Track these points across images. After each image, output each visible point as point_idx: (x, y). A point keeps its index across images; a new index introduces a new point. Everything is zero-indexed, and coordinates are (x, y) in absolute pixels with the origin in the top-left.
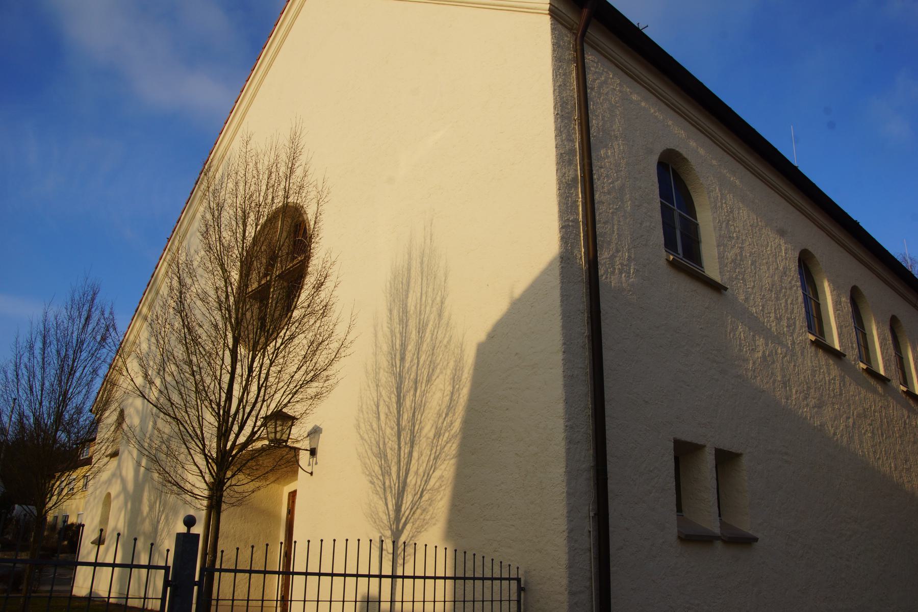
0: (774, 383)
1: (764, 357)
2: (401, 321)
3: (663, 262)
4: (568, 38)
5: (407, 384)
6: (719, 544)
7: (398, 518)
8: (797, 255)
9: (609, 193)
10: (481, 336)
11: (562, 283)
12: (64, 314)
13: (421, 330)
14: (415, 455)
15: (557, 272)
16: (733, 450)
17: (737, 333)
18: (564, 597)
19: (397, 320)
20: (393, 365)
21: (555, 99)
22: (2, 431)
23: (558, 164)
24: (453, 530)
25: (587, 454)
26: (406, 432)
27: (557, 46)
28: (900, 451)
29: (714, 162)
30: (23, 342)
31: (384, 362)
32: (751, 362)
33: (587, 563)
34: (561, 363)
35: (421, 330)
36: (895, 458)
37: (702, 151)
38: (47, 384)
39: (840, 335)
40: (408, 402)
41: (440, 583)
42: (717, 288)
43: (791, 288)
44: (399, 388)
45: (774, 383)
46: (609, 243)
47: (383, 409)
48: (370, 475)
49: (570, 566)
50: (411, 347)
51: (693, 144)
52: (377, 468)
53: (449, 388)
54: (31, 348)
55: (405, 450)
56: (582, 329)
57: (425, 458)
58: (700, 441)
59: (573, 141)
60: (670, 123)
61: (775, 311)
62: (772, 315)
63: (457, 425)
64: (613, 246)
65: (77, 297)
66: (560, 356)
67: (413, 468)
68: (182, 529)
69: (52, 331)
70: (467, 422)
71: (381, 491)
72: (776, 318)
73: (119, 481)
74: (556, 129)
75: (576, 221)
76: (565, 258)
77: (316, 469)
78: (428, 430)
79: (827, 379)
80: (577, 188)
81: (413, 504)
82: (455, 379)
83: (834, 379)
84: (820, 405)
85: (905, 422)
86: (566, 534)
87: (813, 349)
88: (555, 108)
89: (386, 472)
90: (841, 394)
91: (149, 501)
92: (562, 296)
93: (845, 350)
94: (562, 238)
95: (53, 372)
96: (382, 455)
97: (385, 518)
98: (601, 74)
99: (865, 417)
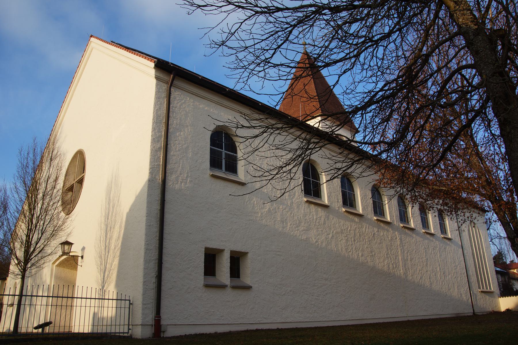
0: (275, 222)
4: (165, 87)
5: (109, 229)
9: (179, 151)
11: (148, 190)
13: (113, 207)
16: (243, 251)
17: (252, 202)
18: (141, 306)
20: (105, 221)
21: (154, 116)
23: (152, 143)
24: (117, 285)
25: (155, 255)
26: (107, 248)
27: (157, 92)
28: (367, 248)
31: (103, 221)
33: (152, 294)
35: (113, 207)
36: (363, 250)
39: (328, 197)
40: (108, 236)
41: (80, 296)
42: (243, 184)
44: (106, 230)
47: (102, 239)
50: (110, 214)
55: (107, 255)
56: (157, 207)
57: (111, 257)
60: (222, 114)
63: (120, 244)
66: (145, 218)
70: (122, 243)
75: (160, 165)
76: (151, 181)
77: (83, 264)
78: (113, 247)
79: (315, 218)
81: (108, 275)
82: (120, 227)
84: (308, 230)
85: (374, 234)
87: (307, 204)
89: (101, 264)
90: (324, 224)
92: (148, 195)
93: (331, 203)
94: (150, 173)
96: (101, 257)
97: (100, 281)
98: (182, 100)
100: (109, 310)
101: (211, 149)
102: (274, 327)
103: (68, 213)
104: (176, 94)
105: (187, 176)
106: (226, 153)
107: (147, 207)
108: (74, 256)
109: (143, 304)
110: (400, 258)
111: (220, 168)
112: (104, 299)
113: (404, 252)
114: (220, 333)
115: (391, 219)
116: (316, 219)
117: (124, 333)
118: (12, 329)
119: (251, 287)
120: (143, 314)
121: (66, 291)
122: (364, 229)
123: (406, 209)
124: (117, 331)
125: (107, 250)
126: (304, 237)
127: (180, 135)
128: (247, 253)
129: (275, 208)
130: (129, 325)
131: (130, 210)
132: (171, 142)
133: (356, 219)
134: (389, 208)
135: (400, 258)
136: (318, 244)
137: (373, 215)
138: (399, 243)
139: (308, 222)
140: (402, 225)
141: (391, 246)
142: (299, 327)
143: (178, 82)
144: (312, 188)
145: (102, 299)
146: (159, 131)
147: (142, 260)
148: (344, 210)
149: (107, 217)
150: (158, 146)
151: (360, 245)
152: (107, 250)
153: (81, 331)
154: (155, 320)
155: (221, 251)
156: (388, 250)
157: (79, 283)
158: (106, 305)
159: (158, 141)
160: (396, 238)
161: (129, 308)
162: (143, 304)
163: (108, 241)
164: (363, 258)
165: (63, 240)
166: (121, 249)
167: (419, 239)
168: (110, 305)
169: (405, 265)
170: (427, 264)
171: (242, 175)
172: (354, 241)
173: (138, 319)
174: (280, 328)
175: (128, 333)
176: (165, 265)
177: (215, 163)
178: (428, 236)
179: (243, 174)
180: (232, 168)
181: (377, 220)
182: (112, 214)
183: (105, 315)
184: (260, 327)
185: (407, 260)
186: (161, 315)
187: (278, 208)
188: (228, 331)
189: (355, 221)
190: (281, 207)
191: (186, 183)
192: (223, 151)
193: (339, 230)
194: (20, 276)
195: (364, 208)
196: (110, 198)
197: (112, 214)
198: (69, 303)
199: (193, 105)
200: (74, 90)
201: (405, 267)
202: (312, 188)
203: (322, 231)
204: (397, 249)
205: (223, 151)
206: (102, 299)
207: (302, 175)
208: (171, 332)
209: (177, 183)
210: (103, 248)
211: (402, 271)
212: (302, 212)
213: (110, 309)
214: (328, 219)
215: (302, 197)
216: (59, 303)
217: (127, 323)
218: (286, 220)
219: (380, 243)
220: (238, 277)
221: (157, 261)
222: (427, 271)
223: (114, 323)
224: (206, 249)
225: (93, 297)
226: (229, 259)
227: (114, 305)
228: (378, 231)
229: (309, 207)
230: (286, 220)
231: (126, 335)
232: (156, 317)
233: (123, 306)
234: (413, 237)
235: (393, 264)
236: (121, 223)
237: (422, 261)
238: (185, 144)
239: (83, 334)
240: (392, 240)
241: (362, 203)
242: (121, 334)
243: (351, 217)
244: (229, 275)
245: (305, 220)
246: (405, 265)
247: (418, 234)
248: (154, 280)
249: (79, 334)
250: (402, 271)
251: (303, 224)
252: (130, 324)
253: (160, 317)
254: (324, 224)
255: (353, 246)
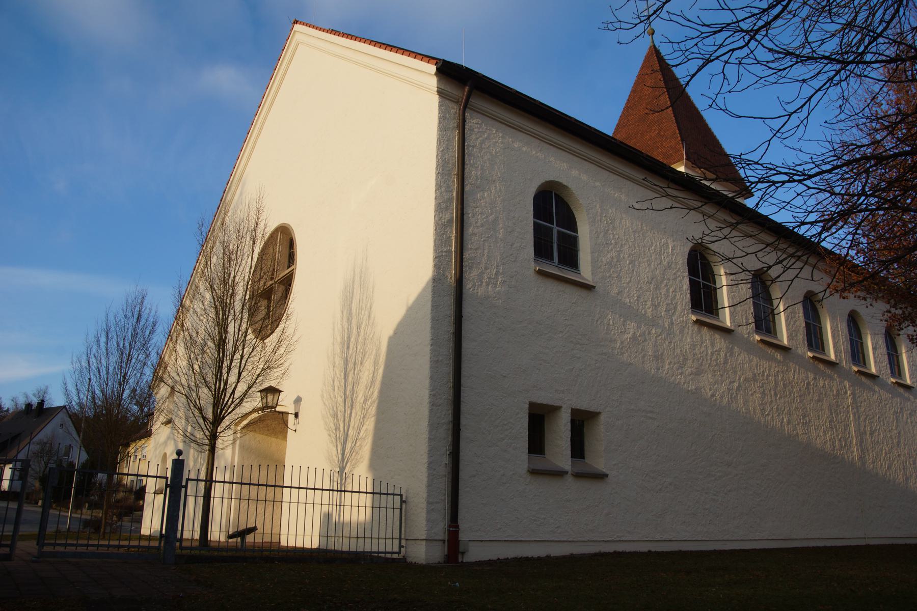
0: (643, 357)
1: (634, 337)
2: (348, 319)
3: (531, 272)
4: (454, 109)
5: (351, 365)
6: (569, 479)
7: (343, 459)
8: (687, 249)
9: (482, 226)
10: (390, 332)
11: (433, 297)
12: (121, 315)
13: (359, 327)
14: (353, 415)
15: (430, 289)
16: (592, 410)
17: (606, 321)
18: (424, 505)
19: (345, 320)
20: (343, 352)
21: (438, 161)
22: (914, 341)
23: (436, 211)
24: (373, 465)
26: (349, 400)
27: (442, 119)
28: (797, 408)
29: (597, 184)
30: (92, 339)
31: (338, 351)
32: (619, 342)
33: (444, 485)
34: (429, 352)
36: (790, 414)
37: (584, 177)
38: (111, 369)
40: (350, 379)
42: (588, 288)
43: (675, 279)
44: (346, 369)
45: (643, 357)
46: (479, 263)
48: (328, 430)
49: (429, 485)
51: (575, 173)
52: (332, 425)
53: (372, 369)
54: (98, 341)
55: (348, 412)
56: (448, 327)
58: (557, 404)
59: (452, 191)
60: (552, 159)
61: (653, 299)
62: (649, 303)
63: (376, 394)
64: (483, 266)
65: (130, 301)
66: (428, 349)
67: (352, 425)
68: (175, 457)
69: (113, 328)
70: (381, 392)
71: (334, 441)
72: (653, 305)
73: (173, 442)
74: (436, 184)
75: (451, 251)
76: (437, 280)
77: (298, 428)
78: (360, 398)
79: (709, 351)
80: (452, 226)
81: (352, 448)
82: (376, 363)
83: (719, 351)
84: (698, 373)
85: (808, 384)
86: (426, 465)
87: (696, 327)
88: (437, 169)
89: (337, 428)
90: (726, 362)
91: (194, 457)
92: (432, 306)
94: (435, 266)
95: (115, 359)
96: (335, 416)
97: (336, 459)
99: (755, 380)
100: (357, 511)
101: (535, 223)
102: (644, 548)
103: (262, 334)
104: (473, 122)
105: (498, 272)
106: (559, 232)
107: (432, 328)
108: (282, 413)
109: (429, 503)
110: (853, 429)
111: (550, 258)
112: (345, 491)
113: (859, 418)
114: (557, 558)
115: (836, 356)
116: (712, 354)
117: (392, 553)
118: (197, 536)
119: (607, 475)
120: (428, 520)
121: (263, 473)
122: (791, 374)
123: (861, 338)
124: (382, 549)
125: (348, 403)
126: (692, 387)
127: (483, 198)
128: (599, 413)
129: (644, 333)
130: (400, 539)
131: (395, 333)
132: (469, 211)
133: (778, 356)
134: (833, 336)
135: (853, 429)
136: (716, 400)
137: (806, 348)
138: (850, 401)
139: (698, 360)
140: (855, 369)
141: (838, 406)
142: (684, 549)
143: (477, 102)
144: (703, 298)
145: (341, 491)
146: (448, 191)
147: (424, 425)
148: (757, 338)
149: (346, 344)
150: (448, 217)
151: (785, 403)
152: (348, 403)
153: (299, 544)
154: (449, 531)
155: (554, 410)
156: (832, 414)
157: (290, 459)
158: (348, 502)
159: (447, 208)
160: (846, 393)
161: (401, 509)
162: (429, 503)
163: (349, 388)
164: (791, 426)
165: (266, 385)
166: (379, 403)
167: (885, 395)
168: (362, 503)
169: (861, 442)
170: (899, 442)
171: (586, 271)
172: (776, 395)
173: (420, 526)
174: (653, 550)
175: (399, 553)
176: (465, 434)
177: (542, 250)
178: (901, 390)
179: (590, 269)
180: (570, 258)
181: (814, 357)
182: (357, 341)
183: (347, 518)
184: (620, 548)
185: (865, 433)
186: (460, 522)
187: (649, 333)
188: (568, 554)
189: (775, 360)
190: (653, 331)
191: (495, 285)
192: (554, 224)
193: (750, 375)
194: (207, 448)
195: (791, 334)
196: (350, 309)
197: (357, 341)
198: (270, 496)
199: (502, 143)
200: (265, 119)
201: (861, 445)
202: (703, 298)
203: (722, 376)
204: (848, 412)
205: (555, 228)
206: (341, 491)
207: (687, 273)
208: (475, 554)
209: (481, 285)
210: (340, 400)
211: (855, 453)
212: (689, 340)
213: (355, 509)
214: (731, 355)
215: (688, 314)
216: (262, 496)
217: (397, 535)
218: (662, 354)
219: (819, 401)
220: (582, 456)
221: (450, 426)
222: (899, 456)
223: (368, 534)
224: (532, 405)
225: (326, 487)
226: (569, 424)
227: (369, 504)
228: (815, 379)
229: (699, 331)
230: (662, 354)
231: (395, 556)
232: (450, 526)
233: (383, 504)
234: (874, 391)
235: (840, 440)
236: (377, 356)
237: (891, 437)
238: (492, 214)
239: (303, 550)
240: (838, 395)
241: (787, 326)
242: (389, 556)
243: (770, 351)
244: (569, 452)
245: (694, 355)
246: (861, 442)
247: (883, 385)
248: (446, 460)
249: (295, 549)
250: (855, 453)
251: (690, 362)
252: (403, 537)
253: (457, 527)
254: (726, 362)
255: (773, 404)
